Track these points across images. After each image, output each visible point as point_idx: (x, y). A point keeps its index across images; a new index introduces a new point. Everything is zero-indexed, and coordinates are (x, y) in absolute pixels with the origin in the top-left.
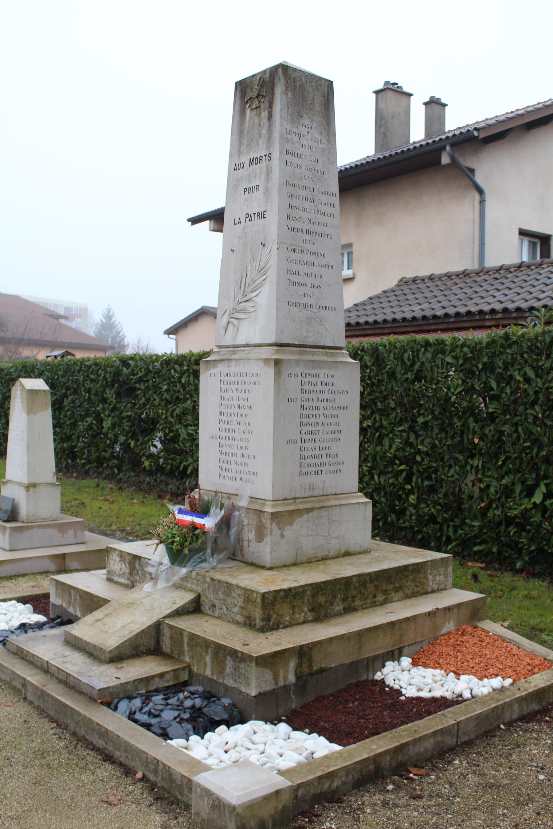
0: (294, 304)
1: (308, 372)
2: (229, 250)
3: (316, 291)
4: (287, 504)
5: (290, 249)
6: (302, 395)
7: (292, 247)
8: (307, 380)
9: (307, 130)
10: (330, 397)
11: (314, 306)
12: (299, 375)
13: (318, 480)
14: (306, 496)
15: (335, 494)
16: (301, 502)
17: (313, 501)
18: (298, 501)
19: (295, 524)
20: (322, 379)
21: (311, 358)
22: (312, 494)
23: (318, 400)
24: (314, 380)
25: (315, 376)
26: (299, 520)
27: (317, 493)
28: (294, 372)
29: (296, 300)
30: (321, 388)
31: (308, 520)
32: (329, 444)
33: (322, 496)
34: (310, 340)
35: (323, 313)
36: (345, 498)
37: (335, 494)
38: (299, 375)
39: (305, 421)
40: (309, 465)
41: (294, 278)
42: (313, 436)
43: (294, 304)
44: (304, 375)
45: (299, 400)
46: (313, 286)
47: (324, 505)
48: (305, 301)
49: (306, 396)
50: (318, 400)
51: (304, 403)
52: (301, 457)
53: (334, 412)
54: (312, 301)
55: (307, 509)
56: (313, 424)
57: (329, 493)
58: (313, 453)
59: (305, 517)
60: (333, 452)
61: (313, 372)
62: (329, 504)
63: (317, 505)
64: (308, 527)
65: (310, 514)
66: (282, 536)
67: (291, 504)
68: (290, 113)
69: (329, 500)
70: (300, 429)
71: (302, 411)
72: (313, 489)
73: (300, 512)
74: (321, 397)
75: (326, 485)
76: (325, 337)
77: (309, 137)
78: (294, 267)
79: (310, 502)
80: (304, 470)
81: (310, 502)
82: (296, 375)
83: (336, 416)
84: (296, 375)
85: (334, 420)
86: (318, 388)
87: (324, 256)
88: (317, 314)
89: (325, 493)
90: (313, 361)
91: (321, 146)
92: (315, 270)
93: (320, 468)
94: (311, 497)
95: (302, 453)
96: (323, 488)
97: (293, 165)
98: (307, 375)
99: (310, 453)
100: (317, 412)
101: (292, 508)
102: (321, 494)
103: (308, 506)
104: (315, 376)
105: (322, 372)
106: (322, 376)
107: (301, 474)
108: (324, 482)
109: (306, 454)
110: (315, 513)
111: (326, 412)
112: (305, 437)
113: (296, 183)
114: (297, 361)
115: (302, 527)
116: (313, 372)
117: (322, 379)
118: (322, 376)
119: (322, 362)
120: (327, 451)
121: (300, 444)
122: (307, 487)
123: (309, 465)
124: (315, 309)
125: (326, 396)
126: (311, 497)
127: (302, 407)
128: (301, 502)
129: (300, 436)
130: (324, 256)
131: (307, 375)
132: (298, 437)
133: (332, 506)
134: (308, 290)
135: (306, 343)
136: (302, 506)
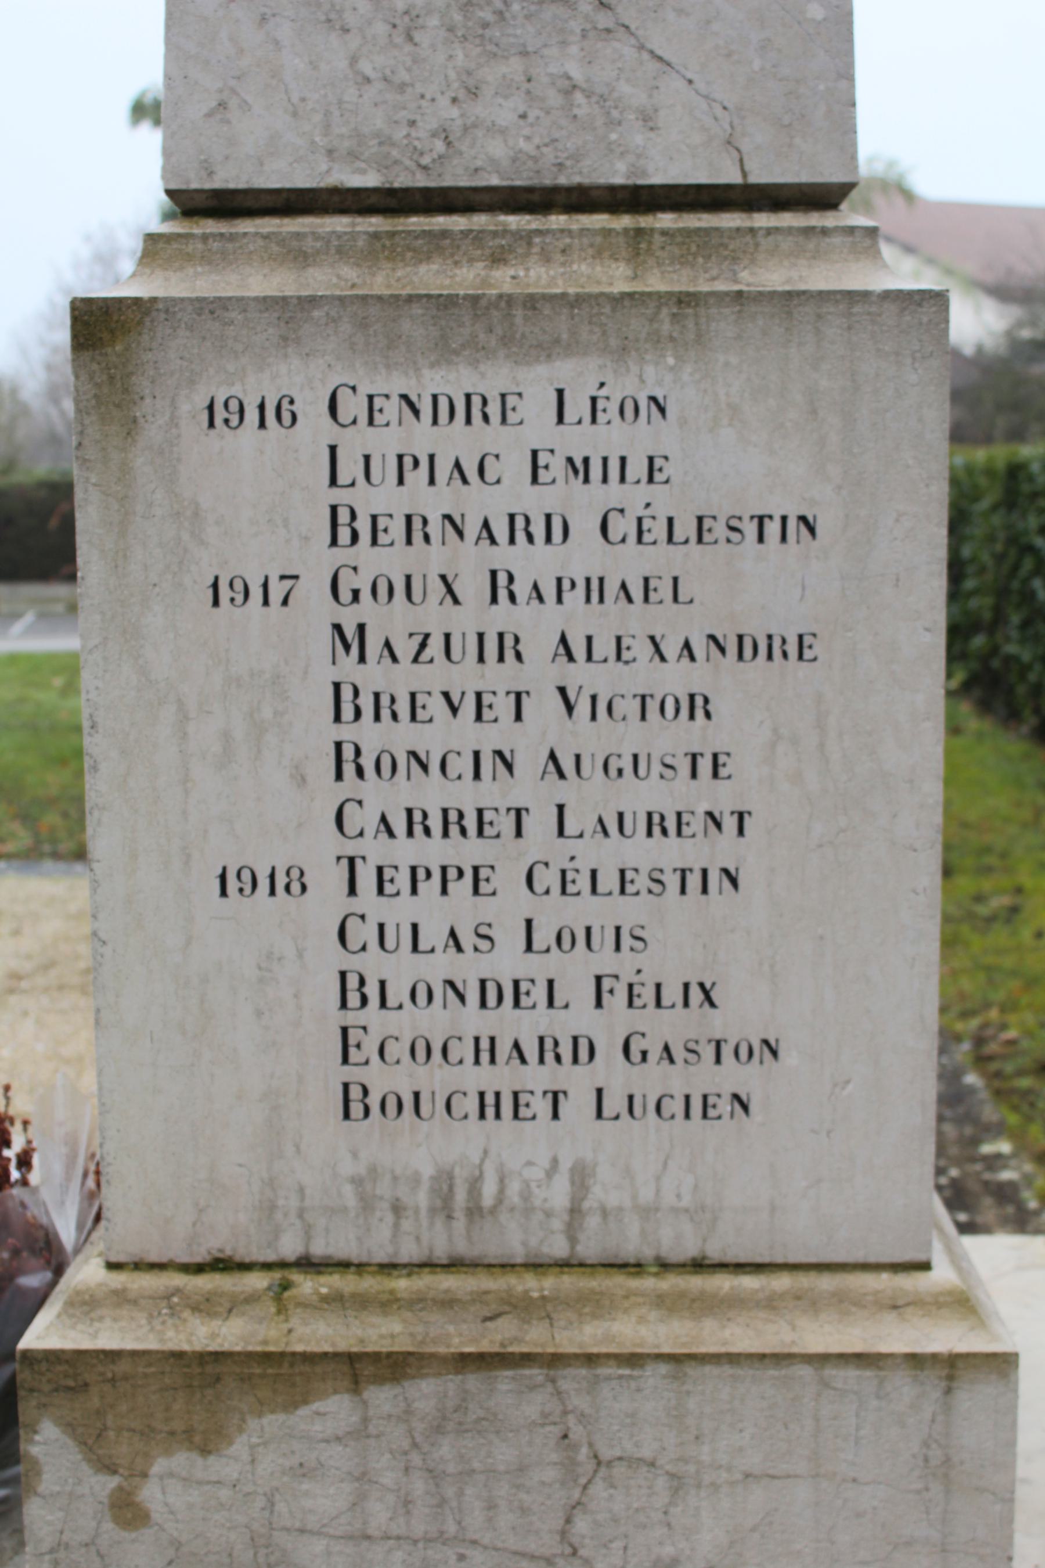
1: (399, 384)
4: (205, 1306)
6: (343, 555)
8: (386, 442)
10: (629, 563)
13: (524, 1156)
14: (409, 1251)
15: (699, 1265)
16: (336, 1300)
17: (448, 1303)
18: (306, 1285)
19: (239, 1447)
21: (465, 277)
22: (462, 1248)
23: (498, 587)
24: (457, 442)
26: (272, 1422)
27: (512, 1239)
30: (534, 502)
31: (361, 1432)
32: (629, 911)
33: (564, 1265)
34: (497, 149)
36: (771, 1303)
37: (699, 1265)
38: (312, 409)
39: (370, 736)
40: (421, 1050)
42: (468, 851)
44: (352, 406)
45: (314, 589)
47: (535, 1337)
49: (372, 562)
50: (498, 587)
51: (367, 610)
52: (349, 989)
53: (675, 679)
55: (351, 1359)
56: (463, 765)
57: (632, 1244)
58: (469, 969)
59: (335, 1410)
60: (669, 962)
61: (453, 381)
62: (587, 1335)
63: (463, 1336)
64: (363, 1477)
65: (382, 1398)
66: (127, 1511)
67: (236, 1304)
69: (596, 1305)
70: (328, 795)
71: (348, 667)
72: (474, 1211)
73: (285, 1376)
74: (531, 563)
75: (597, 1194)
76: (648, 120)
79: (417, 1302)
80: (381, 1080)
81: (417, 1302)
83: (697, 706)
84: (283, 413)
85: (675, 737)
86: (511, 494)
89: (589, 1249)
90: (446, 303)
93: (537, 1078)
94: (455, 1265)
95: (353, 963)
96: (575, 1211)
98: (392, 409)
99: (438, 966)
100: (498, 678)
101: (231, 1334)
102: (558, 1248)
103: (383, 1332)
104: (471, 409)
105: (535, 384)
107: (350, 1102)
108: (581, 1177)
109: (400, 970)
110: (425, 1393)
111: (581, 676)
112: (375, 850)
114: (289, 313)
115: (303, 1471)
116: (453, 381)
119: (532, 302)
120: (604, 960)
121: (339, 904)
122: (422, 1199)
123: (421, 1050)
125: (584, 555)
126: (455, 1265)
127: (351, 641)
128: (336, 1300)
129: (333, 844)
132: (320, 853)
133: (590, 1359)
135: (455, 176)
136: (318, 1333)
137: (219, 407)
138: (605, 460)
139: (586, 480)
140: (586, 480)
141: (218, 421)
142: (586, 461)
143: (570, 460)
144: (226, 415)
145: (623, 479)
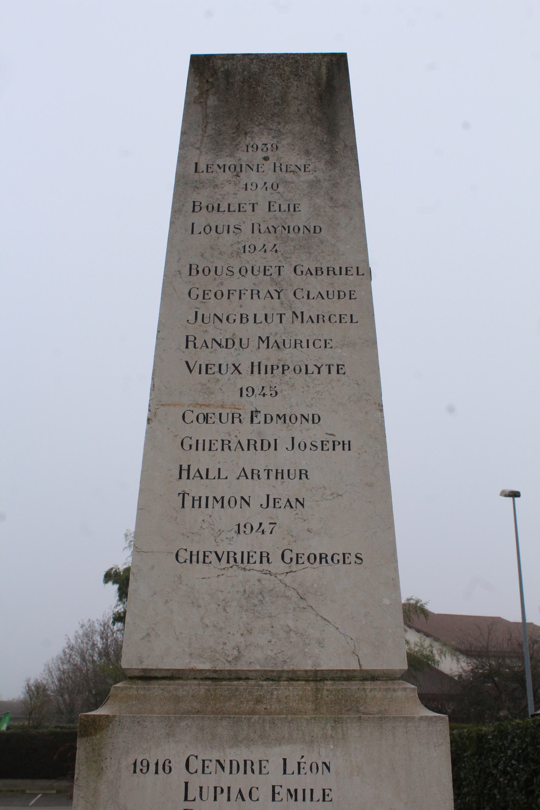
0: (199, 558)
1: (215, 755)
2: (394, 584)
3: (283, 515)
5: (190, 417)
7: (197, 411)
9: (260, 155)
11: (275, 557)
12: (178, 765)
20: (274, 775)
25: (247, 767)
28: (155, 755)
29: (209, 546)
35: (310, 574)
38: (178, 765)
41: (196, 488)
43: (199, 558)
44: (195, 765)
46: (271, 502)
48: (241, 544)
54: (269, 543)
61: (239, 754)
68: (210, 131)
76: (320, 643)
77: (268, 166)
78: (202, 460)
82: (166, 767)
84: (166, 767)
87: (315, 419)
88: (288, 579)
91: (305, 177)
92: (283, 459)
97: (207, 229)
98: (212, 766)
104: (247, 767)
106: (274, 766)
113: (219, 264)
116: (239, 754)
117: (274, 775)
118: (274, 766)
124: (277, 565)
130: (315, 419)
131: (212, 766)
134: (254, 515)
137: (139, 763)
138: (304, 790)
139: (296, 800)
140: (296, 800)
141: (138, 770)
142: (296, 790)
143: (289, 790)
144: (142, 767)
145: (312, 799)
